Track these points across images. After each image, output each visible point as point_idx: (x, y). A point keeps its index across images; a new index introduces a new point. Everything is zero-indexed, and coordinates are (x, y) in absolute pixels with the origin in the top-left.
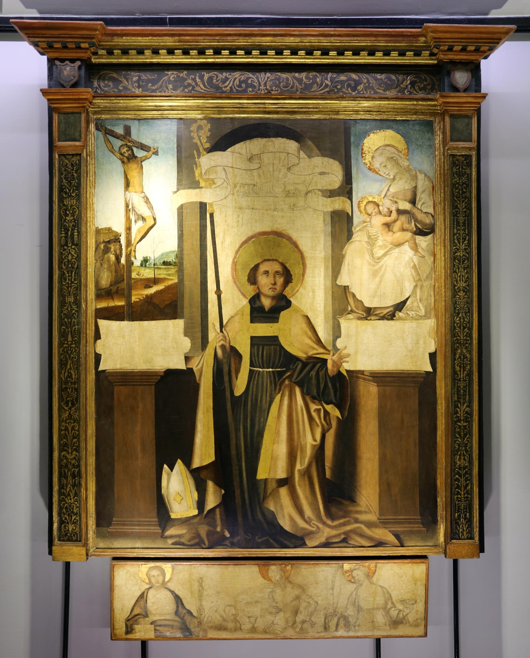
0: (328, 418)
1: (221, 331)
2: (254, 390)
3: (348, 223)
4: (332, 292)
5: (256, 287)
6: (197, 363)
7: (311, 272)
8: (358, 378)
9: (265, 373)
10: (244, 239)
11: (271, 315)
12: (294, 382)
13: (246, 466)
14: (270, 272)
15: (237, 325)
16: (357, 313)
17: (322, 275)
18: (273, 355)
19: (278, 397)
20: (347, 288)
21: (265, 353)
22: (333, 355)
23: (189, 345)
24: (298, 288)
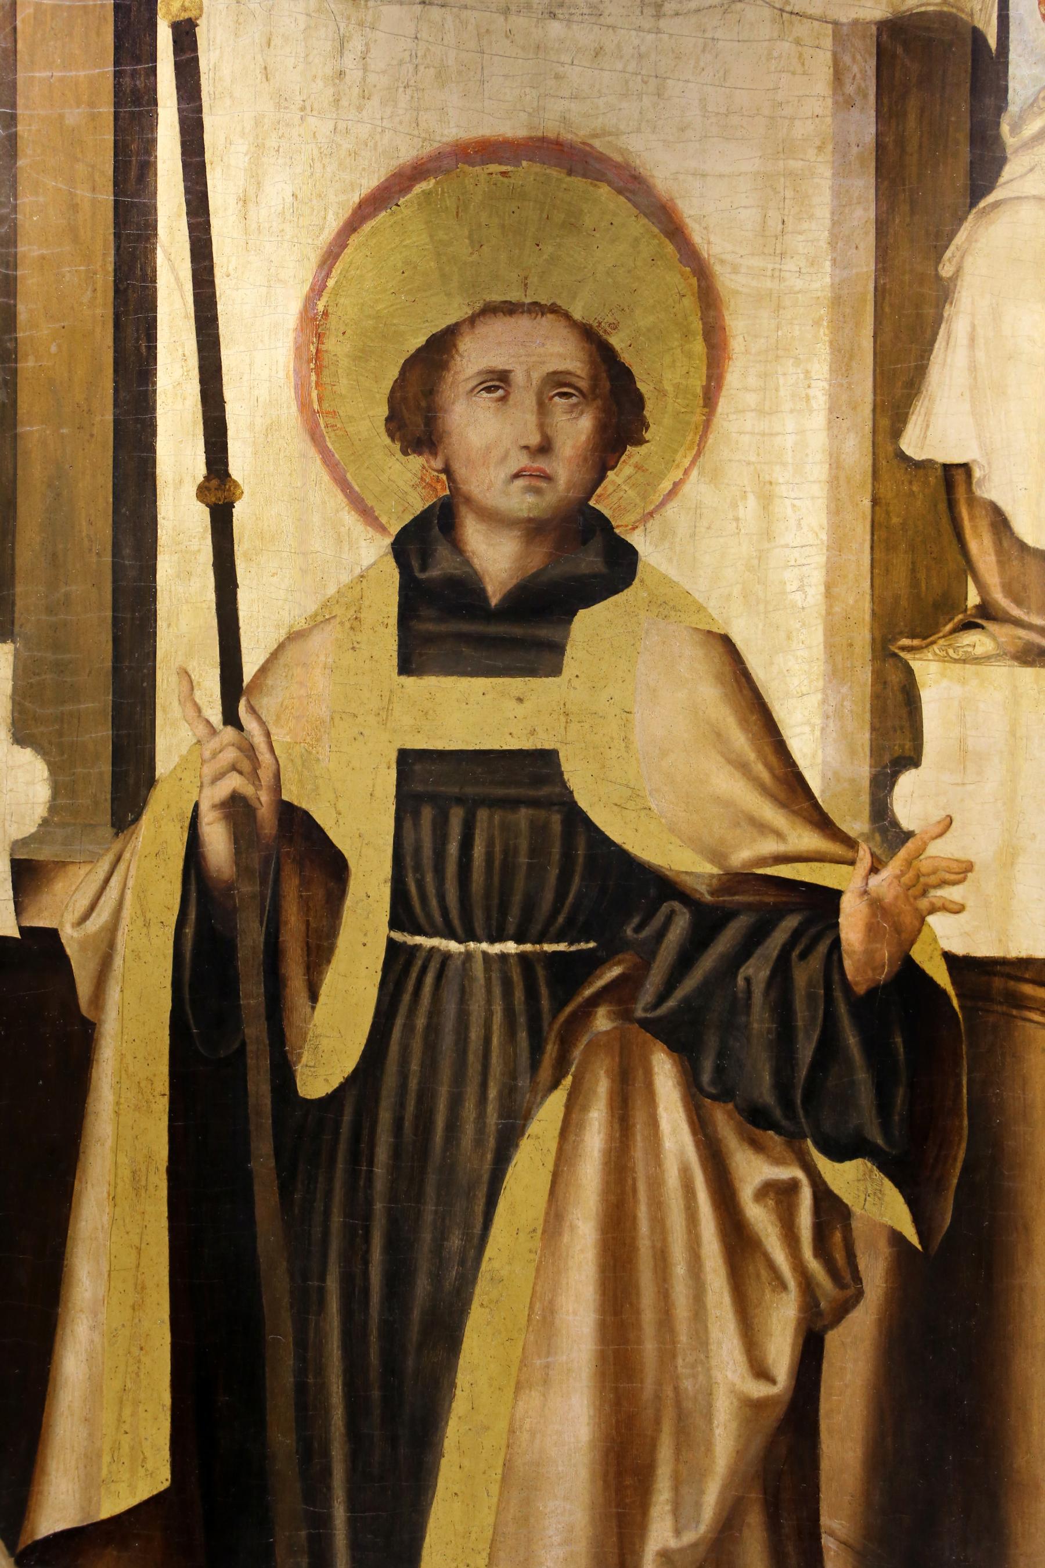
0: (838, 1236)
1: (231, 717)
2: (415, 1066)
3: (976, 91)
4: (875, 502)
5: (438, 463)
6: (83, 903)
7: (752, 381)
8: (1019, 1002)
9: (478, 968)
10: (370, 182)
11: (517, 631)
12: (646, 1024)
13: (353, 1523)
14: (519, 377)
15: (320, 682)
16: (1018, 623)
17: (820, 399)
18: (523, 859)
19: (557, 1100)
20: (959, 476)
21: (478, 851)
22: (874, 870)
23: (42, 793)
24: (677, 475)
